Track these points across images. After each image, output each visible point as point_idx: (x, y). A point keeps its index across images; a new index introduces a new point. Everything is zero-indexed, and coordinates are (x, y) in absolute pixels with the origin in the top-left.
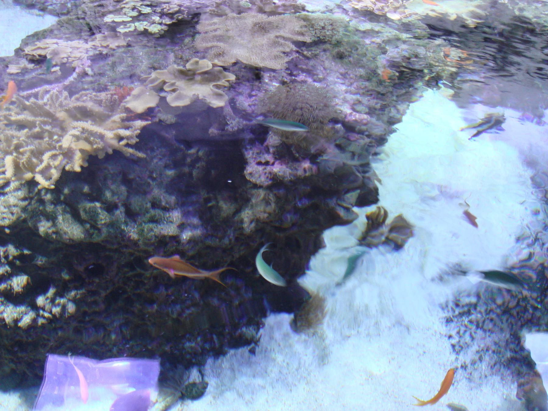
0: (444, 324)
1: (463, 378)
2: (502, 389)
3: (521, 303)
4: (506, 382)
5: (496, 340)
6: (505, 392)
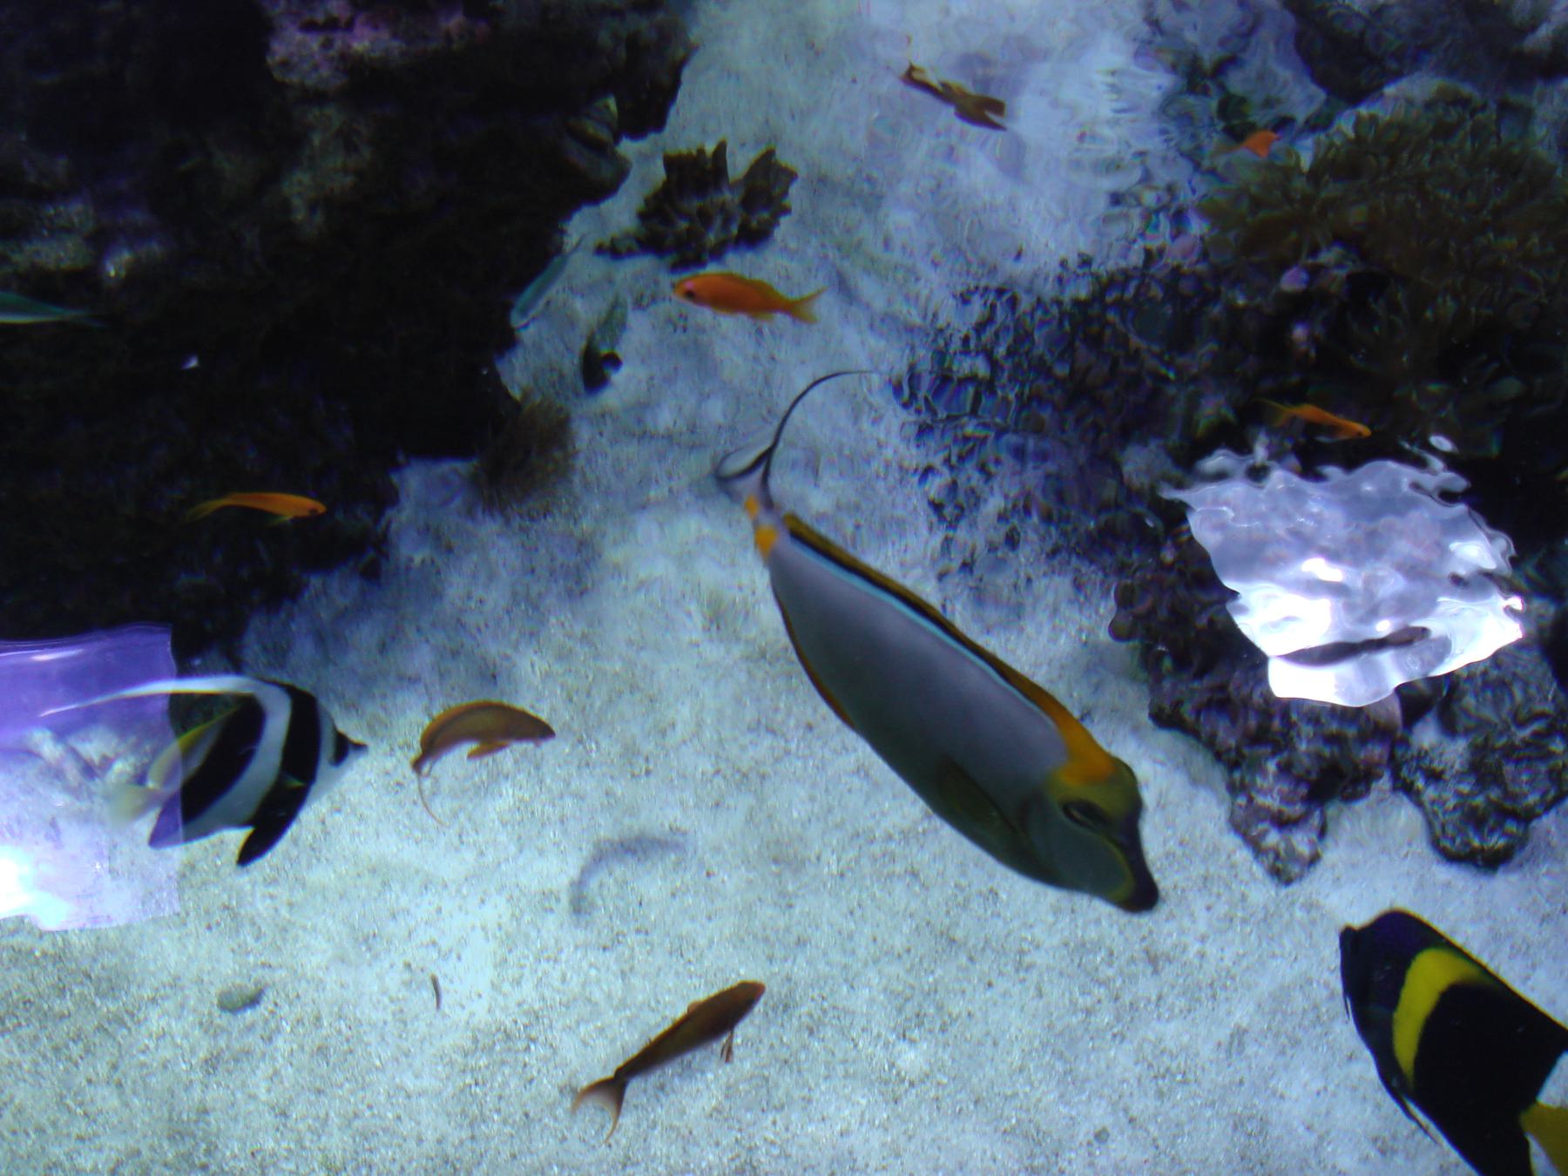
2: (1077, 616)
3: (1123, 367)
4: (1086, 596)
6: (1085, 623)
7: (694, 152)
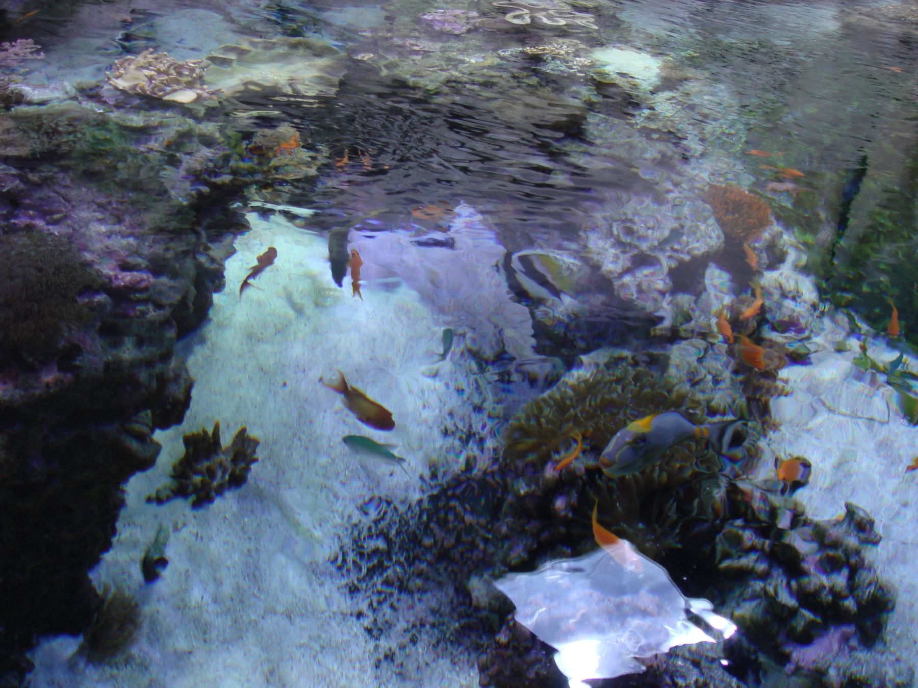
0: (348, 596)
1: (392, 676)
2: (457, 678)
3: (465, 538)
5: (434, 604)
7: (133, 603)
